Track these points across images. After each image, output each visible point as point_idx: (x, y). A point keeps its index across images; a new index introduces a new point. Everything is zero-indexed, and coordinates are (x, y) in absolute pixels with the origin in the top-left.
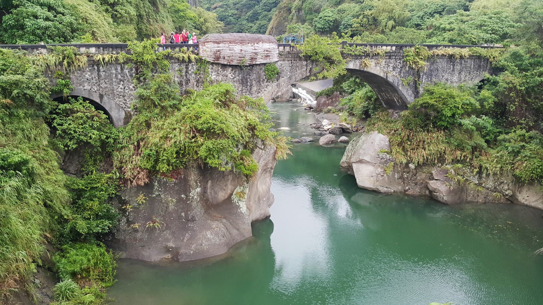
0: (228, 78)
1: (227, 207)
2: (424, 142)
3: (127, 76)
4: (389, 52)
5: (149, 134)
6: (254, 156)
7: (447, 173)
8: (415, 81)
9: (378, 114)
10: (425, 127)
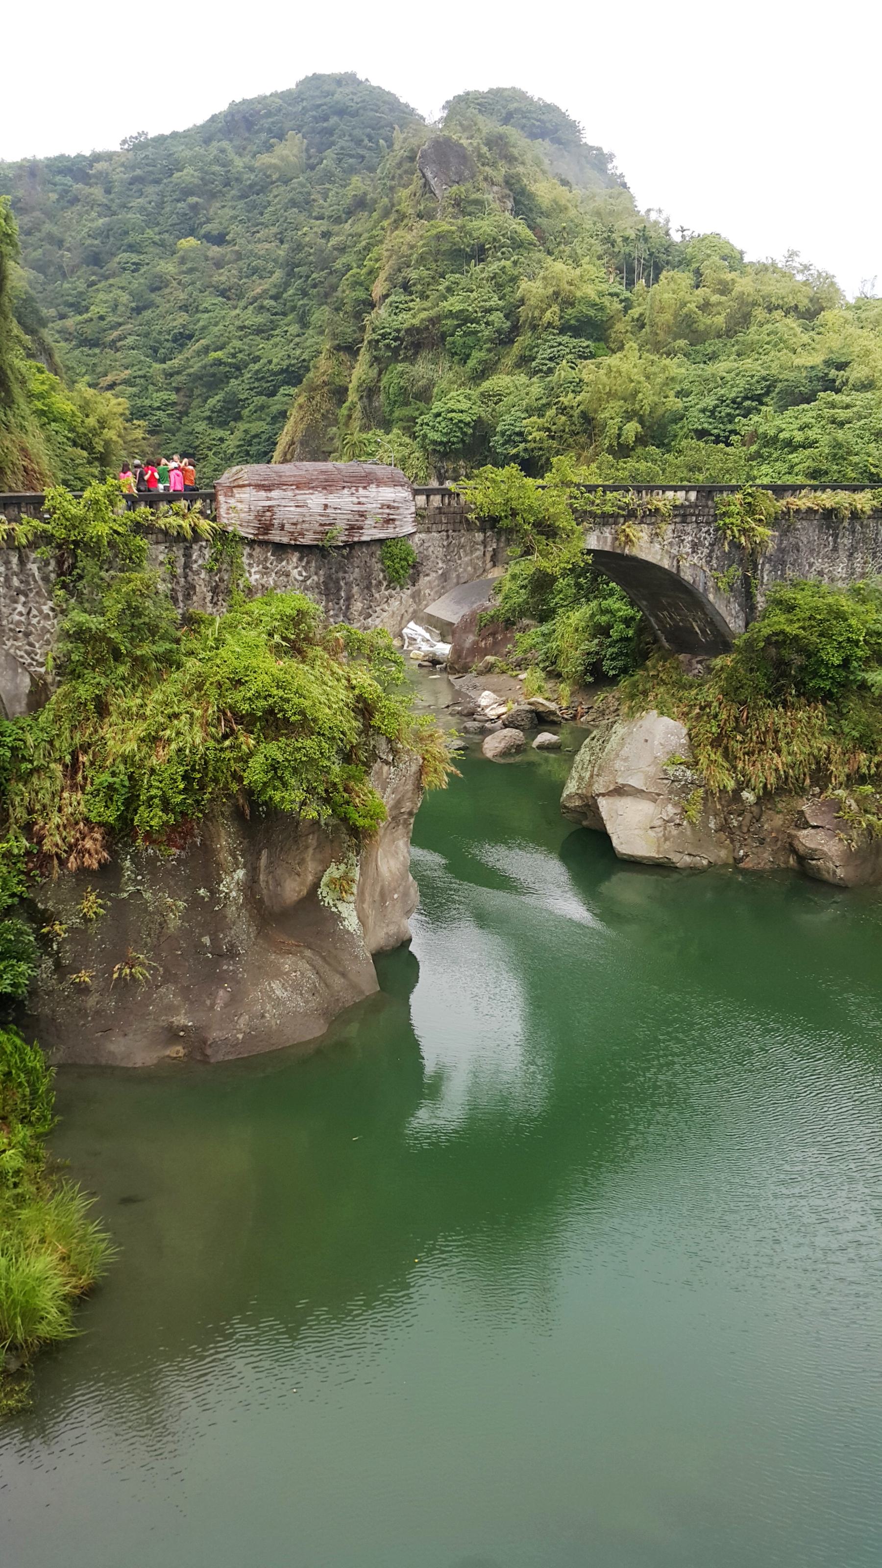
0: (291, 578)
1: (303, 922)
2: (777, 732)
3: (36, 581)
4: (682, 506)
5: (107, 732)
6: (370, 783)
7: (840, 809)
8: (746, 578)
9: (654, 667)
10: (776, 696)
